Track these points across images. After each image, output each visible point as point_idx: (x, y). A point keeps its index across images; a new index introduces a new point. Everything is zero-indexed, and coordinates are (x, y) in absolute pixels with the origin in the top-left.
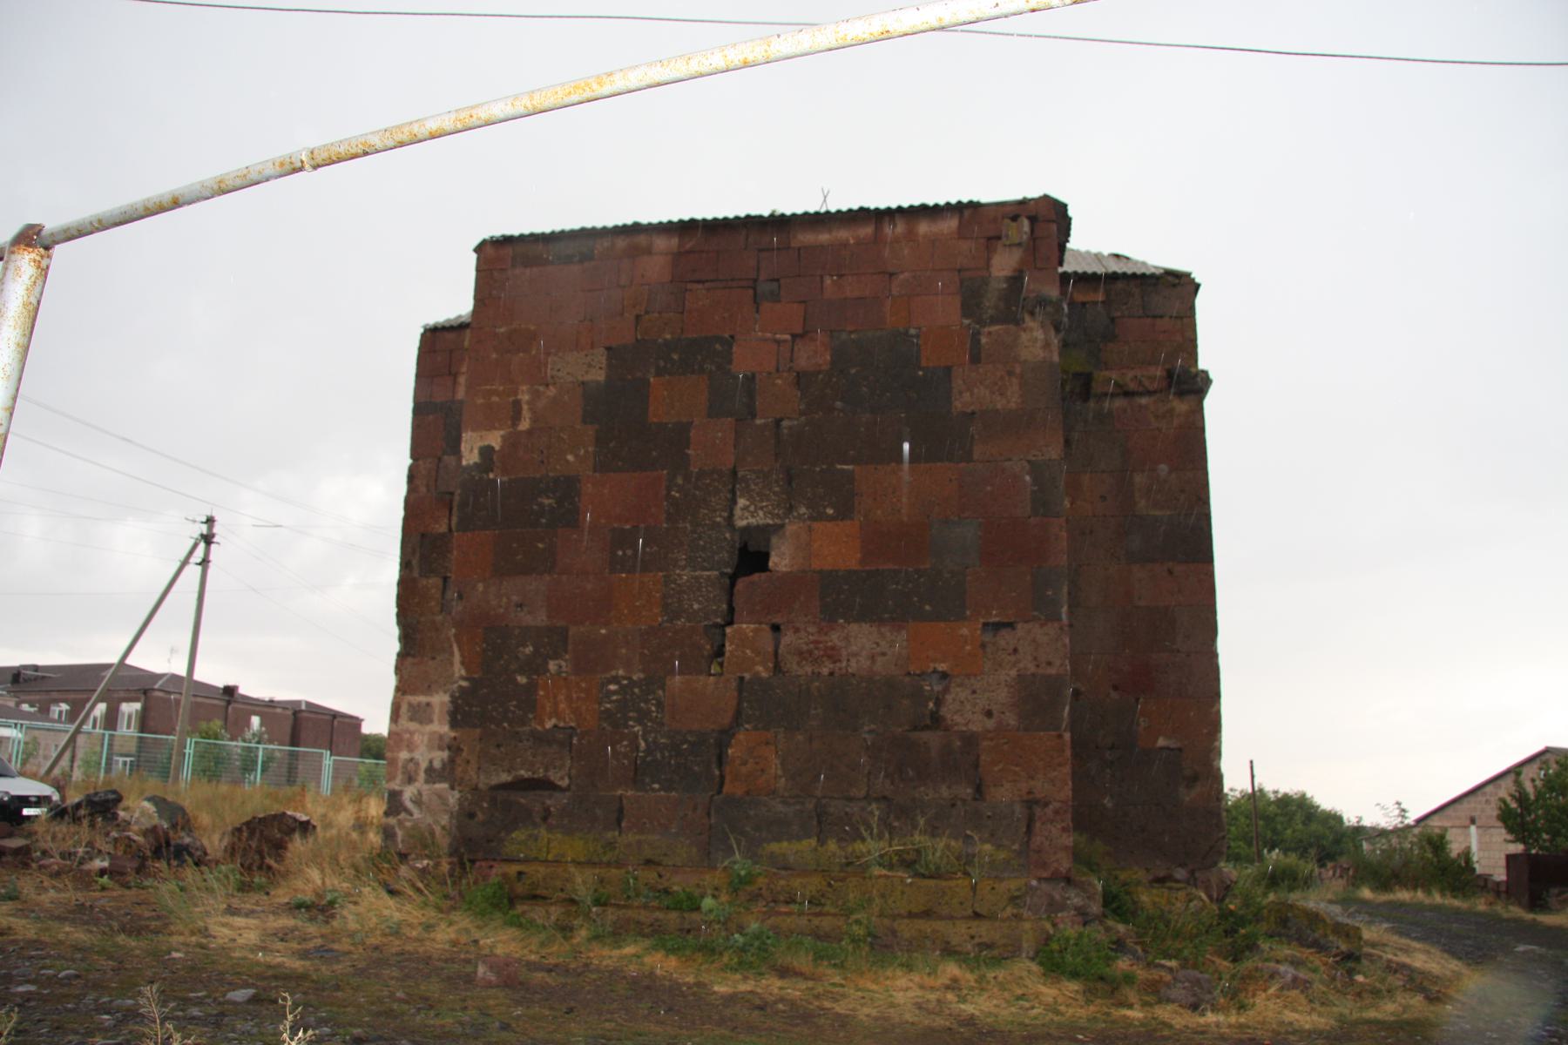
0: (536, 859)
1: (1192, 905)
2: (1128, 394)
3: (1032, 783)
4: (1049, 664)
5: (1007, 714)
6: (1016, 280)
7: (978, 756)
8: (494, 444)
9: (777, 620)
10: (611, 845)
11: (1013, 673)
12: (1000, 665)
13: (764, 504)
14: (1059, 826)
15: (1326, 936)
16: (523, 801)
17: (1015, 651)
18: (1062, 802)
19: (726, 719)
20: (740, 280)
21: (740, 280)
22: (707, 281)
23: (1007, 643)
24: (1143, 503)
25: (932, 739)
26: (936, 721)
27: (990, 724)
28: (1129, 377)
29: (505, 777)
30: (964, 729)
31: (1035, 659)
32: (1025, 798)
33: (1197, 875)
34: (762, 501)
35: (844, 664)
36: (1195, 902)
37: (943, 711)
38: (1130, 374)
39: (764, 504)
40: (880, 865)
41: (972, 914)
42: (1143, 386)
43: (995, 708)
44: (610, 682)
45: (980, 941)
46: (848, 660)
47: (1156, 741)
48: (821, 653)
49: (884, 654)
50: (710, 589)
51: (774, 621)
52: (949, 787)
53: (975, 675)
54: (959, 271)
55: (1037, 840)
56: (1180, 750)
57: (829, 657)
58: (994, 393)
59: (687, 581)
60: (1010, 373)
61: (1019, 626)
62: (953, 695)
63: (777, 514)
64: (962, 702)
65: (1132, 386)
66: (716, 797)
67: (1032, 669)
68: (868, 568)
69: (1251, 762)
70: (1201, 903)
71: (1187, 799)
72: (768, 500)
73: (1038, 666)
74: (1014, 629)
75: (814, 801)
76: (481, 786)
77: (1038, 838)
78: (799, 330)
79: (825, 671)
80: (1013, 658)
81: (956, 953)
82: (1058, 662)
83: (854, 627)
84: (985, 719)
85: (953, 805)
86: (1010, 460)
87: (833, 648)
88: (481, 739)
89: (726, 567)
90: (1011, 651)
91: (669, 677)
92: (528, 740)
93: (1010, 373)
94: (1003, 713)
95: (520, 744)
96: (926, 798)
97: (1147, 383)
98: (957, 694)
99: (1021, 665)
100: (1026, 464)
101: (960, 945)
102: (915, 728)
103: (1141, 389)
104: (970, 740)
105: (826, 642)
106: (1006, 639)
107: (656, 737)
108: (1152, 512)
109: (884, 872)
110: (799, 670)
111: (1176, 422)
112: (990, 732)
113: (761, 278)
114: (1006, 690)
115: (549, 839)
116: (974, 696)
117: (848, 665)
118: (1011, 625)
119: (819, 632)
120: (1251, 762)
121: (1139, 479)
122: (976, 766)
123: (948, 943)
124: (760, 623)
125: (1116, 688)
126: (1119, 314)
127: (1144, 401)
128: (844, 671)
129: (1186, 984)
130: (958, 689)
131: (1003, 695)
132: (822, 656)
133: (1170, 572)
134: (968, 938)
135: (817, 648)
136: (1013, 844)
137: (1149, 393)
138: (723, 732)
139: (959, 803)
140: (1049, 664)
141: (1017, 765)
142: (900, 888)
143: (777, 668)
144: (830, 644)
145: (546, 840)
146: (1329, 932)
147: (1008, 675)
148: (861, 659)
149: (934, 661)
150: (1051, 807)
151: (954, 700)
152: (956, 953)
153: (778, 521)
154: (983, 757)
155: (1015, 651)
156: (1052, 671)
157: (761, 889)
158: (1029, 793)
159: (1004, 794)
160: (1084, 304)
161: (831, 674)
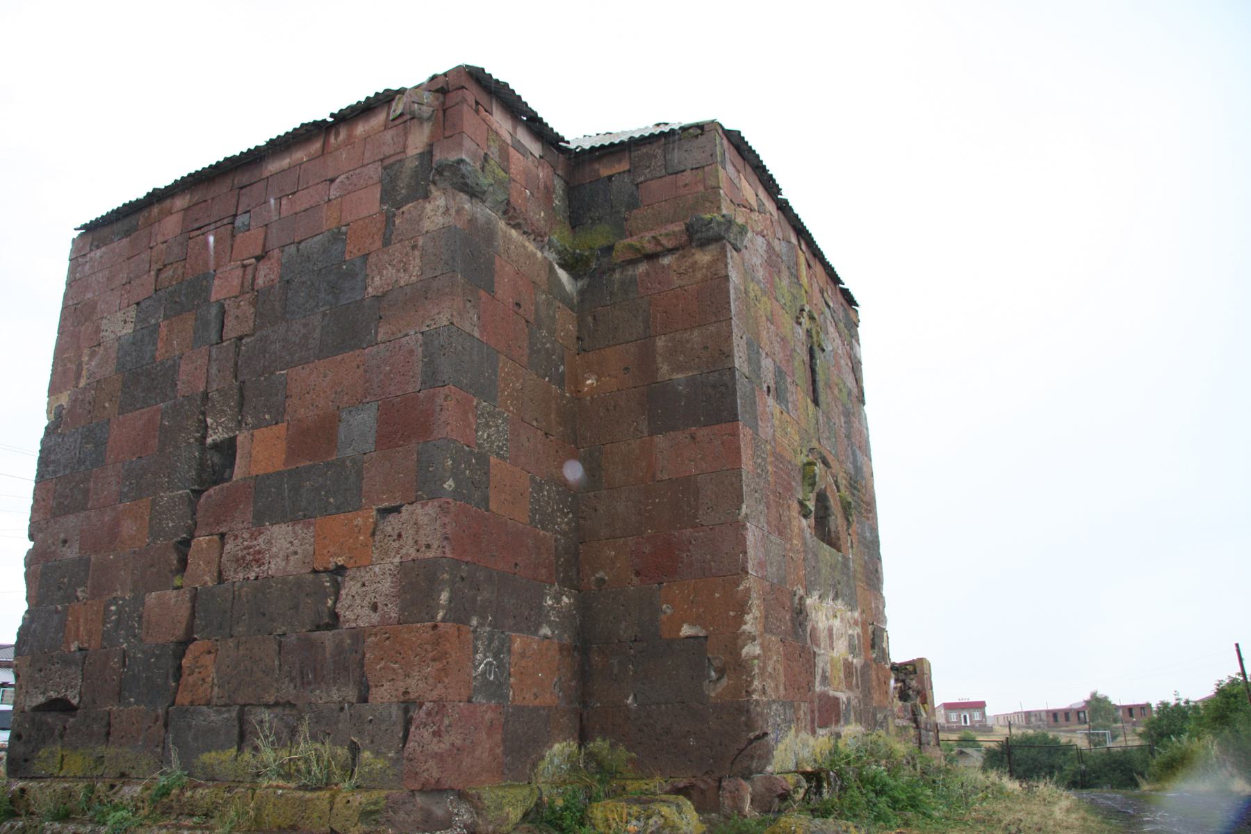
1: (651, 822)
2: (651, 257)
4: (428, 546)
6: (428, 154)
9: (223, 530)
11: (397, 560)
12: (386, 554)
13: (223, 420)
17: (400, 536)
18: (434, 702)
19: (180, 632)
20: (215, 222)
21: (215, 222)
22: (203, 227)
24: (665, 368)
25: (327, 637)
26: (334, 620)
27: (375, 618)
29: (41, 699)
31: (416, 542)
32: (402, 699)
34: (221, 417)
35: (266, 567)
36: (655, 818)
37: (340, 609)
38: (648, 236)
39: (223, 420)
40: (279, 775)
42: (661, 245)
43: (380, 601)
44: (111, 604)
48: (251, 557)
49: (296, 553)
51: (221, 530)
52: (338, 690)
54: (382, 160)
57: (257, 561)
60: (414, 247)
62: (346, 590)
63: (231, 428)
65: (650, 248)
68: (289, 468)
69: (1237, 645)
70: (662, 820)
71: (713, 694)
73: (418, 551)
75: (237, 708)
76: (27, 708)
79: (252, 576)
80: (396, 544)
86: (406, 335)
87: (259, 552)
88: (30, 666)
89: (194, 485)
90: (395, 537)
91: (147, 594)
93: (414, 247)
94: (386, 605)
96: (320, 702)
98: (350, 588)
99: (403, 551)
102: (318, 628)
103: (659, 249)
104: (358, 635)
105: (255, 546)
106: (392, 524)
107: (135, 653)
109: (281, 783)
110: (236, 576)
111: (699, 275)
113: (239, 213)
115: (63, 756)
116: (364, 589)
117: (269, 568)
118: (397, 510)
119: (251, 538)
120: (1237, 645)
124: (212, 535)
125: (638, 574)
126: (642, 179)
127: (666, 261)
128: (265, 574)
130: (352, 583)
131: (386, 585)
133: (693, 438)
136: (390, 751)
137: (670, 251)
138: (179, 643)
140: (428, 546)
141: (396, 662)
143: (220, 579)
144: (258, 548)
147: (392, 563)
151: (347, 595)
153: (232, 435)
154: (368, 656)
155: (400, 536)
156: (430, 554)
158: (406, 693)
159: (384, 694)
160: (610, 178)
161: (257, 578)
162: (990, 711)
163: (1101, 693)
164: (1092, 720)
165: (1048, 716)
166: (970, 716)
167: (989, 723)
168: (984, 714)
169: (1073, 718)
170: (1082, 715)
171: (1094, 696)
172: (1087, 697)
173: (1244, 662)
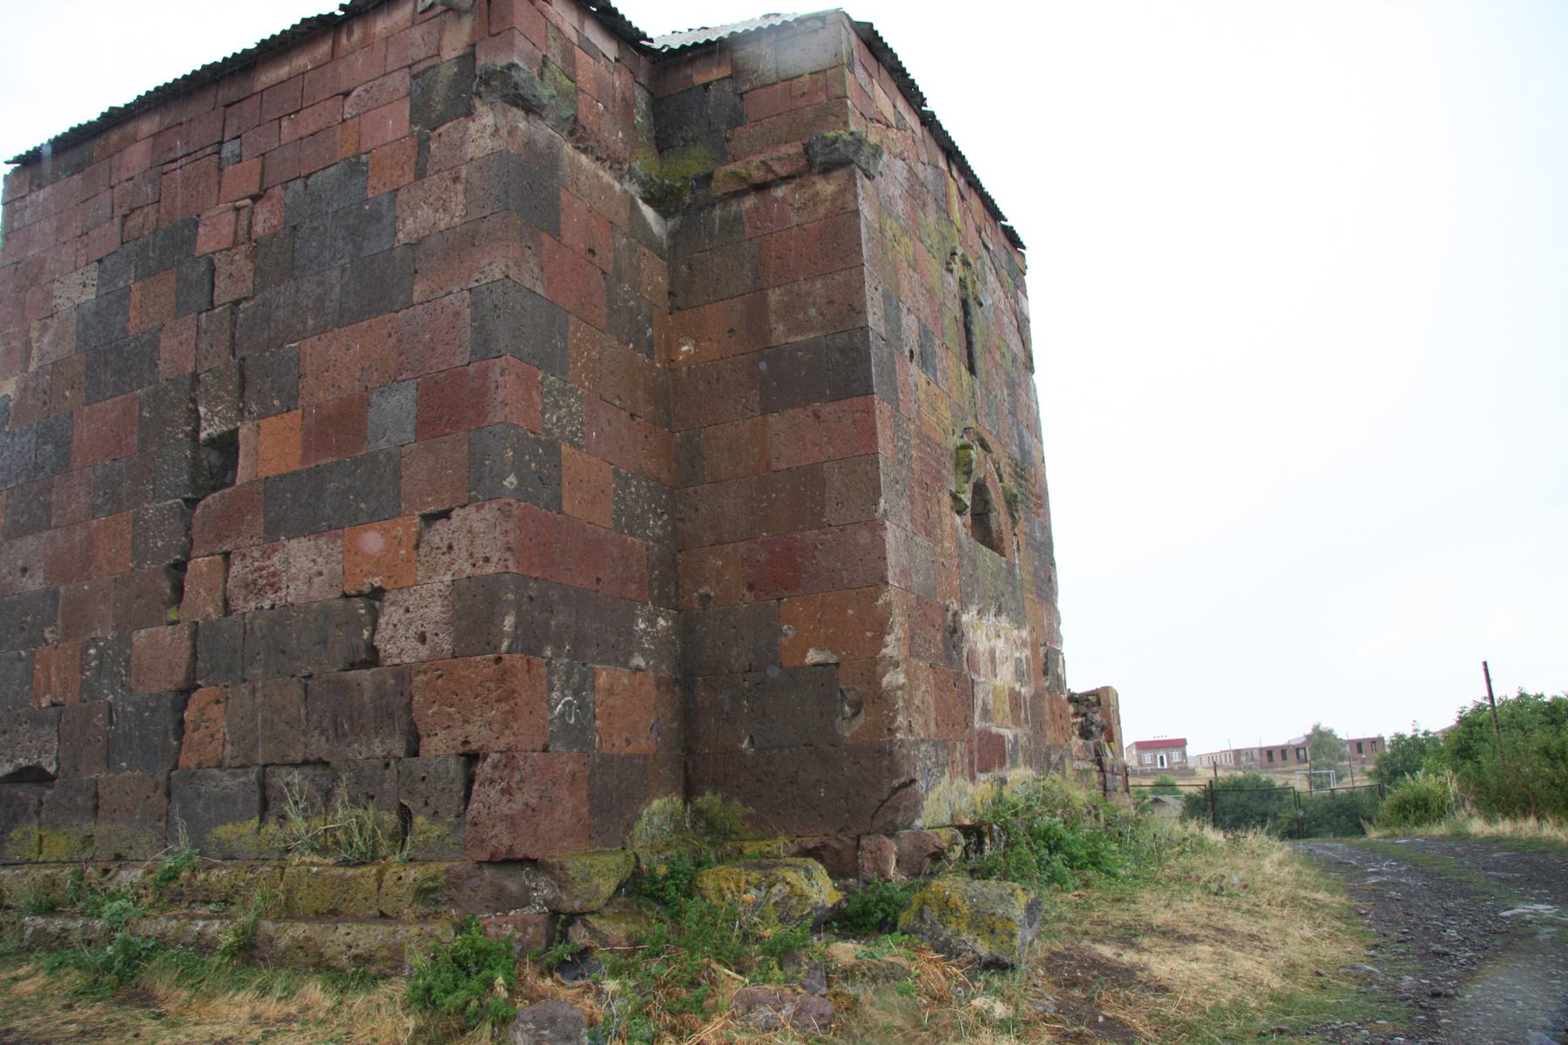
0: (29, 861)
1: (774, 890)
3: (468, 728)
4: (487, 560)
5: (441, 636)
7: (411, 698)
8: (10, 393)
10: (88, 840)
11: (448, 578)
13: (220, 408)
14: (498, 788)
15: (958, 933)
16: (21, 794)
17: (450, 547)
18: (501, 752)
23: (442, 539)
26: (372, 657)
27: (424, 651)
28: (752, 167)
30: (397, 661)
31: (471, 555)
32: (461, 750)
33: (863, 842)
36: (779, 886)
37: (379, 642)
38: (756, 160)
40: (313, 849)
41: (378, 914)
42: (773, 171)
43: (429, 629)
45: (357, 952)
46: (288, 587)
47: (804, 656)
48: (265, 581)
49: (320, 574)
50: (171, 520)
51: (224, 549)
53: (408, 587)
55: (474, 806)
56: (837, 664)
58: (437, 211)
59: (154, 515)
61: (454, 514)
62: (386, 618)
64: (395, 625)
65: (758, 176)
66: (173, 773)
67: (469, 570)
70: (788, 889)
72: (223, 403)
73: (474, 565)
74: (449, 518)
77: (475, 805)
78: (255, 190)
79: (267, 604)
80: (446, 558)
81: (329, 968)
82: (495, 557)
83: (294, 543)
84: (419, 645)
85: (387, 766)
86: (450, 293)
87: (274, 574)
90: (445, 549)
92: (26, 722)
94: (437, 635)
95: (20, 728)
97: (777, 167)
98: (391, 615)
99: (456, 567)
100: (466, 294)
101: (335, 958)
102: (353, 666)
103: (770, 177)
104: (403, 674)
108: (791, 340)
110: (246, 605)
111: (822, 211)
112: (424, 662)
113: (226, 139)
114: (439, 603)
115: (41, 836)
116: (408, 615)
118: (445, 515)
121: (774, 296)
122: (409, 709)
123: (321, 955)
124: (213, 554)
125: (751, 587)
126: (748, 87)
129: (530, 1026)
130: (393, 608)
131: (436, 610)
132: (265, 585)
133: (817, 416)
134: (344, 948)
135: (261, 577)
139: (393, 762)
140: (487, 560)
141: (452, 706)
142: (306, 880)
143: (227, 609)
145: (37, 836)
146: (964, 926)
147: (442, 582)
148: (298, 583)
149: (370, 574)
150: (489, 760)
151: (387, 624)
152: (329, 968)
154: (416, 698)
155: (450, 547)
156: (490, 569)
157: (182, 885)
158: (466, 743)
160: (706, 86)
161: (273, 607)
162: (1191, 751)
163: (1325, 726)
164: (1314, 758)
165: (1261, 754)
166: (1168, 757)
167: (1191, 764)
168: (1184, 754)
169: (1291, 756)
170: (1302, 752)
171: (1316, 730)
172: (1309, 731)
173: (1492, 684)
